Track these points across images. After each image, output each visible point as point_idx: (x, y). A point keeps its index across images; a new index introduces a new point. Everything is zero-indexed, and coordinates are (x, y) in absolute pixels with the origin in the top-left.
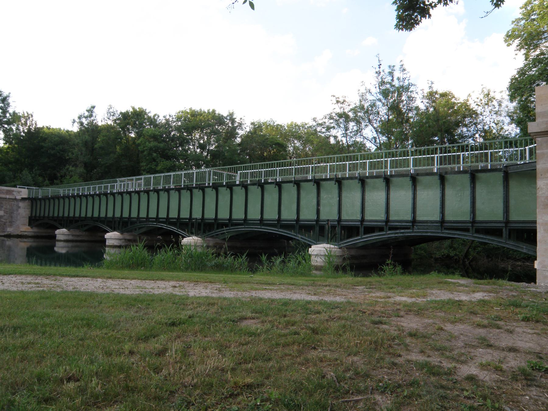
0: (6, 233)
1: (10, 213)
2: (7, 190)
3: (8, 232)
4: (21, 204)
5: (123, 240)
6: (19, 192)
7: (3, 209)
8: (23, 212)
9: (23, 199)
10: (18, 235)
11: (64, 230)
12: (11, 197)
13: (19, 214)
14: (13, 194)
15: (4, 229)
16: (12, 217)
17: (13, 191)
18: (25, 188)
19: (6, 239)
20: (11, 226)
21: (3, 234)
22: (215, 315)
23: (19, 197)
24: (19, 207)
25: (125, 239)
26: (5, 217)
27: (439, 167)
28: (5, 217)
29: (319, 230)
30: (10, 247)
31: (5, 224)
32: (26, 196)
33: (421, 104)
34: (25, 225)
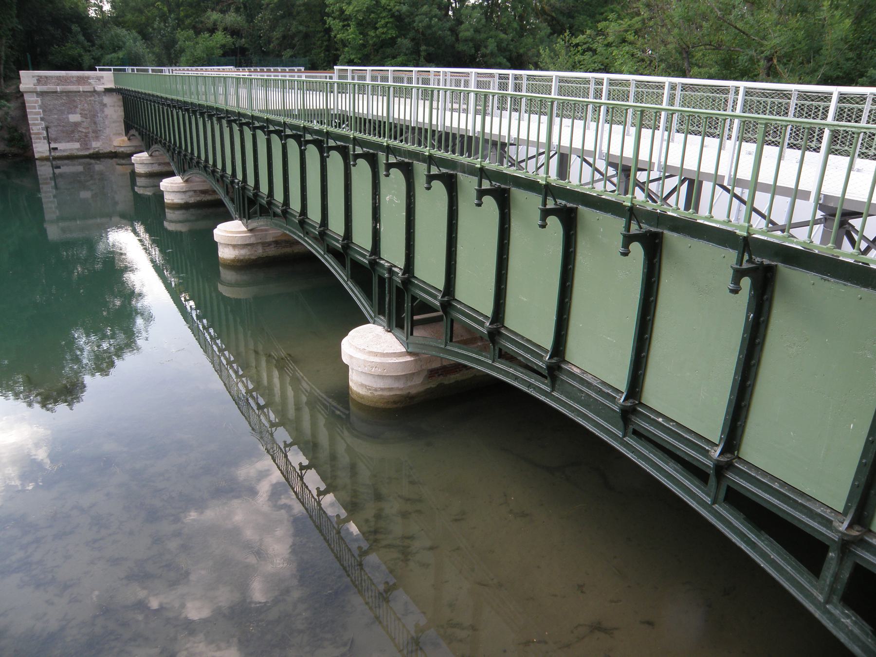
0: (91, 151)
1: (92, 116)
2: (78, 77)
3: (94, 148)
4: (107, 99)
5: (191, 193)
6: (99, 79)
7: (78, 110)
8: (113, 112)
9: (108, 91)
10: (111, 152)
11: (144, 155)
12: (87, 88)
13: (106, 116)
14: (90, 84)
15: (87, 144)
16: (95, 123)
17: (88, 78)
18: (110, 70)
19: (93, 161)
20: (97, 138)
21: (87, 153)
22: (602, 11)
23: (100, 88)
24: (105, 105)
25: (195, 191)
26: (85, 125)
27: (702, 116)
28: (85, 125)
29: (398, 302)
30: (101, 173)
31: (86, 136)
32: (111, 85)
33: (139, 305)
34: (119, 134)
